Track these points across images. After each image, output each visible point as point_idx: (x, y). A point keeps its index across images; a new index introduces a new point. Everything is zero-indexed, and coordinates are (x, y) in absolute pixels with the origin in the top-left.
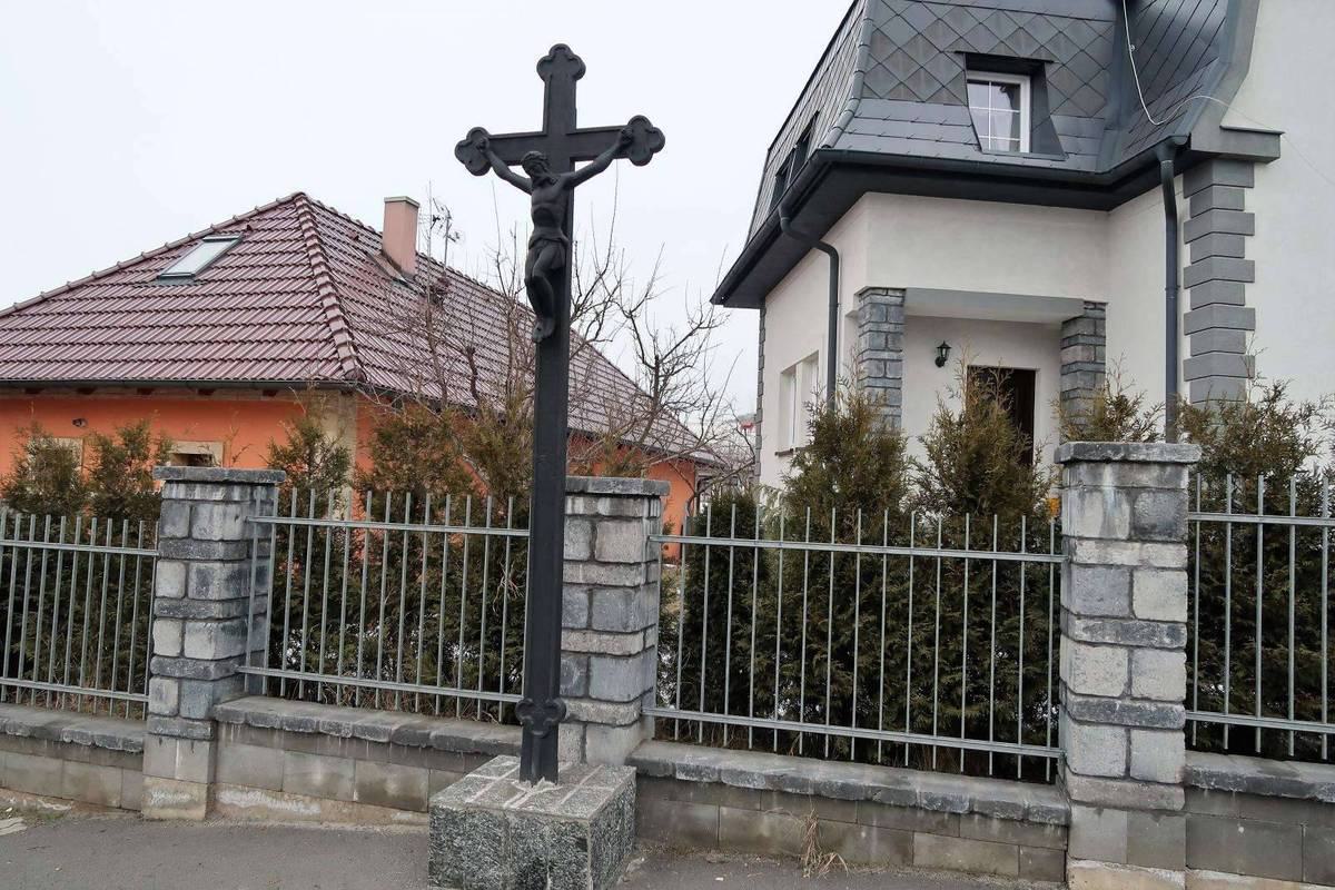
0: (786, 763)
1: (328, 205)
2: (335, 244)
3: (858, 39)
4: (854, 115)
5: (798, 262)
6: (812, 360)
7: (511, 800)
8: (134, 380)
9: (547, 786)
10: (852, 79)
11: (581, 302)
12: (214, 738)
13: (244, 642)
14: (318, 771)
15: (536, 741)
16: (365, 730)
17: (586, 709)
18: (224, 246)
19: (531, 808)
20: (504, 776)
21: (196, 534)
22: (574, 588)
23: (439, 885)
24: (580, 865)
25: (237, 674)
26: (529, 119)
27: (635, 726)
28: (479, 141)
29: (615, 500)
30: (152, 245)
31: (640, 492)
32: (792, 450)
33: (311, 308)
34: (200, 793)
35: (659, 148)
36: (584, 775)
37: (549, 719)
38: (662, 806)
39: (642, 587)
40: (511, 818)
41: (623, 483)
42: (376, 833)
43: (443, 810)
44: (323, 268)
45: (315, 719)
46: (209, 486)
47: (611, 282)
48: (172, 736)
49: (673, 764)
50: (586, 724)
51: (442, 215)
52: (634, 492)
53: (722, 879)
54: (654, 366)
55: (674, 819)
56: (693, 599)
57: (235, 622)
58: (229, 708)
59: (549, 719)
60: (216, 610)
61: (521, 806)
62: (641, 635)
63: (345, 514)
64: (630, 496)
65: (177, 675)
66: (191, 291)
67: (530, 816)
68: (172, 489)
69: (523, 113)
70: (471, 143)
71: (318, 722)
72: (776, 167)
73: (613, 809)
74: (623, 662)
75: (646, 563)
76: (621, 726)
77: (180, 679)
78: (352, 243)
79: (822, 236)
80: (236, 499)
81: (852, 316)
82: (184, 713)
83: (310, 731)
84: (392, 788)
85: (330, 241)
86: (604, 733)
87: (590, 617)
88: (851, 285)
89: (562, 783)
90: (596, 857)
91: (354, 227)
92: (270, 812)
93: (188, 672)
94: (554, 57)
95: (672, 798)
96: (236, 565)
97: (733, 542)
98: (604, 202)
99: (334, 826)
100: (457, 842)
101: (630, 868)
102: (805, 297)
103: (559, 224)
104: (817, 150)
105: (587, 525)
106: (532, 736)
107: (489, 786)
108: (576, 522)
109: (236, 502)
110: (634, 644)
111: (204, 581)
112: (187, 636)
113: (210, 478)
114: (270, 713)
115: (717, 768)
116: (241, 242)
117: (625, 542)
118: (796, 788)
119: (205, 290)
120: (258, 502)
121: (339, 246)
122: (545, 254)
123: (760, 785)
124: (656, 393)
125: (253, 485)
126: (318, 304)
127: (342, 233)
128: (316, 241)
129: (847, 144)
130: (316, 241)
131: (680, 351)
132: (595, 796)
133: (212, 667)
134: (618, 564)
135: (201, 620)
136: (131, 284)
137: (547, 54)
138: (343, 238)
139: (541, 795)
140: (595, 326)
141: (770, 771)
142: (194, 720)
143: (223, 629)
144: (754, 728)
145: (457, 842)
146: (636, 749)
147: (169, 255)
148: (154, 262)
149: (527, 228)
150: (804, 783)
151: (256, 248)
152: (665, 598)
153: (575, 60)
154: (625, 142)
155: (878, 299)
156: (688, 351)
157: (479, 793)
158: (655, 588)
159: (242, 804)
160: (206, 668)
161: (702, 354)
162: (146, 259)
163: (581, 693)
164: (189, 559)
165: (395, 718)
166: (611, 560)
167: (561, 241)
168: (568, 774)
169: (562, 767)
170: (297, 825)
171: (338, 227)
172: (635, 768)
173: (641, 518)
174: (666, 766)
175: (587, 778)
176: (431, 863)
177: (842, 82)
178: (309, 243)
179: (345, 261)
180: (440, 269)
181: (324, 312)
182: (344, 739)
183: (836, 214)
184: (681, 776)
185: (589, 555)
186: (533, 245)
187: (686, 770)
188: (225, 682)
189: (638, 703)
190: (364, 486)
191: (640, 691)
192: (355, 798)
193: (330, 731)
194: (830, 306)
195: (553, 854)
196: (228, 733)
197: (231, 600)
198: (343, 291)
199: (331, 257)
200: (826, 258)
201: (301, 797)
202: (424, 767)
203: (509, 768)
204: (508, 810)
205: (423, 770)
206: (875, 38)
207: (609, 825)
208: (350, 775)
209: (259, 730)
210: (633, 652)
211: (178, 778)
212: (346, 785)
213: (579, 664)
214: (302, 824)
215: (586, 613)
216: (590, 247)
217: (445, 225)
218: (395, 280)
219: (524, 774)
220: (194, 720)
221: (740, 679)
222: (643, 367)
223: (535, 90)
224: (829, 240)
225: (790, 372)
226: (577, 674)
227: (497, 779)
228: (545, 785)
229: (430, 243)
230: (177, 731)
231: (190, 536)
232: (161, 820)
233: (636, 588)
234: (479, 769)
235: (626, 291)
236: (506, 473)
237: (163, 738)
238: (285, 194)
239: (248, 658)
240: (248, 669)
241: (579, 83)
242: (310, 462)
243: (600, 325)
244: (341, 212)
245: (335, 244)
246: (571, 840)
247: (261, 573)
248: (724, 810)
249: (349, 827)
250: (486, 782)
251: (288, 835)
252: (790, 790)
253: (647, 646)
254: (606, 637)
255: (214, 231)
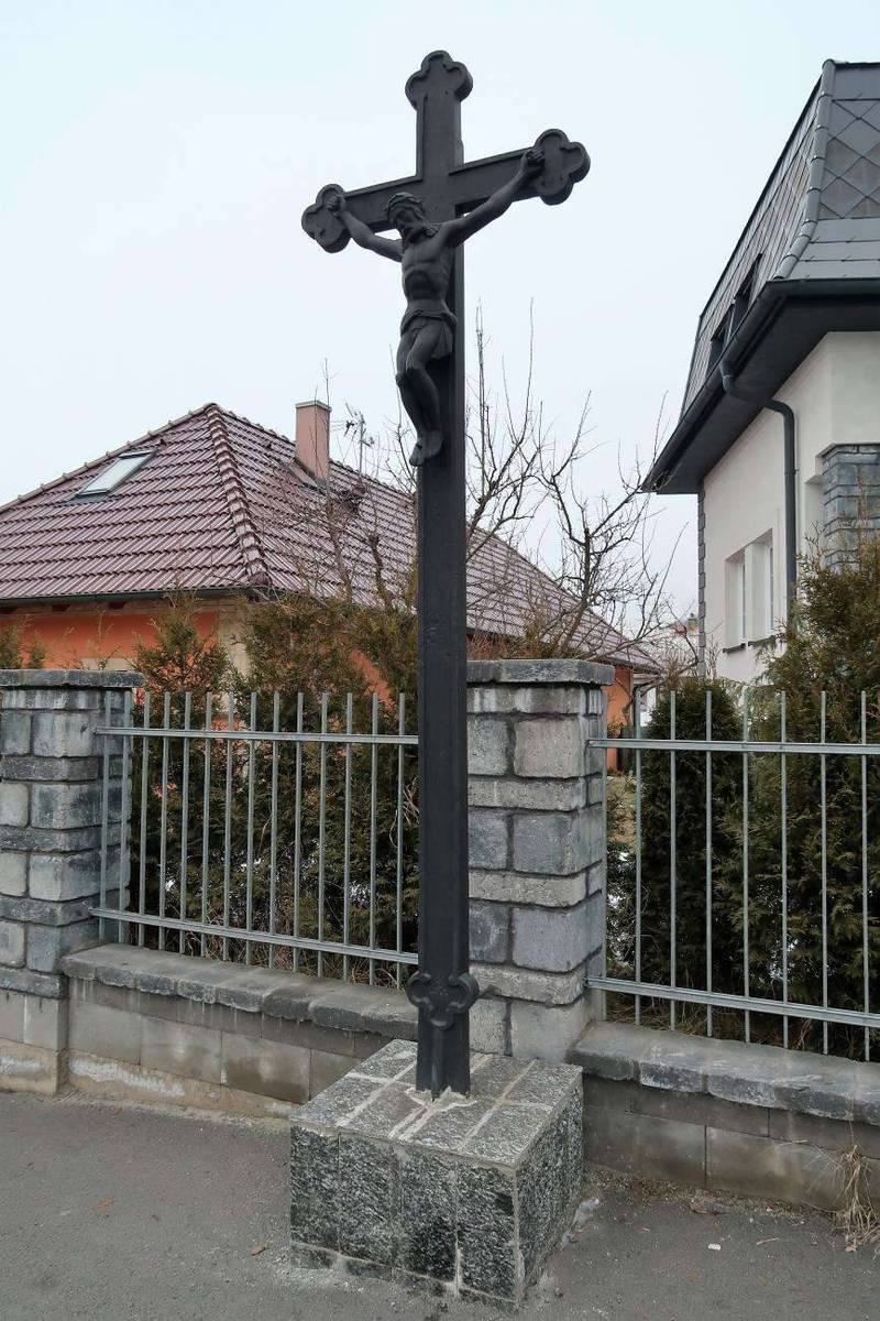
0: (802, 1066)
1: (239, 415)
2: (246, 452)
3: (808, 159)
4: (810, 241)
5: (746, 427)
6: (765, 540)
7: (402, 1125)
8: (48, 597)
9: (456, 1100)
10: (804, 202)
11: (495, 479)
12: (64, 996)
13: (97, 879)
14: (180, 1043)
15: (437, 1035)
16: (231, 995)
17: (511, 982)
18: (139, 460)
19: (428, 1142)
20: (396, 1077)
21: (37, 751)
22: (488, 814)
23: (305, 1241)
24: (503, 1235)
25: (92, 917)
26: (399, 162)
27: (578, 1004)
28: (331, 201)
29: (540, 691)
30: (74, 465)
31: (572, 679)
32: (743, 645)
33: (219, 514)
34: (51, 1063)
35: (581, 172)
36: (507, 1080)
37: (454, 1004)
38: (619, 1119)
39: (580, 811)
40: (400, 1153)
41: (549, 666)
42: (246, 1129)
43: (306, 1134)
44: (231, 474)
45: (173, 978)
46: (49, 692)
47: (528, 449)
48: (19, 991)
49: (636, 1063)
50: (510, 1000)
51: (356, 420)
52: (566, 678)
53: (718, 1247)
54: (583, 541)
55: (638, 1140)
56: (653, 826)
57: (86, 856)
58: (78, 960)
59: (454, 1004)
60: (61, 841)
61: (416, 1137)
62: (582, 877)
63: (232, 731)
64: (559, 685)
65: (23, 918)
66: (106, 506)
67: (427, 1154)
68: (11, 696)
69: (386, 152)
70: (322, 207)
71: (176, 983)
72: (710, 333)
73: (555, 1136)
74: (558, 916)
75: (585, 777)
76: (558, 1006)
77: (26, 923)
78: (264, 450)
79: (775, 392)
80: (82, 707)
81: (815, 483)
82: (31, 964)
83: (168, 993)
84: (266, 1070)
85: (241, 450)
86: (535, 1014)
87: (510, 853)
88: (815, 439)
89: (477, 1093)
90: (528, 1218)
91: (267, 436)
92: (127, 1091)
93: (34, 915)
94: (428, 71)
95: (636, 1109)
96: (85, 788)
97: (709, 745)
98: (503, 258)
99: (201, 1114)
100: (327, 1183)
101: (580, 1217)
102: (754, 472)
103: (442, 294)
104: (767, 283)
105: (501, 726)
106: (431, 1027)
107: (375, 1094)
108: (486, 723)
109: (81, 711)
110: (574, 890)
111: (48, 809)
112: (32, 872)
113: (49, 683)
114: (124, 968)
115: (701, 1072)
116: (154, 456)
117: (556, 748)
118: (826, 1109)
119: (119, 505)
120: (108, 710)
121: (251, 454)
122: (423, 337)
123: (769, 1101)
124: (587, 573)
125: (102, 690)
126: (225, 510)
127: (254, 442)
128: (225, 448)
129: (802, 272)
130: (225, 448)
131: (614, 520)
132: (523, 1121)
133: (59, 909)
134: (546, 780)
135: (45, 853)
136: (52, 504)
137: (419, 68)
138: (256, 447)
139: (445, 1116)
140: (513, 501)
141: (783, 1081)
142: (41, 973)
143: (72, 864)
144: (751, 1012)
145: (327, 1183)
146: (581, 1036)
147: (87, 474)
148: (74, 482)
149: (400, 305)
150: (840, 1104)
151: (168, 461)
152: (613, 822)
153: (458, 69)
154: (532, 169)
155: (847, 457)
156: (624, 519)
157: (359, 1109)
158: (600, 812)
159: (97, 1078)
160: (52, 911)
161: (641, 523)
162: (67, 480)
163: (501, 958)
164: (32, 780)
165: (271, 979)
166: (537, 775)
167: (445, 318)
168: (485, 1075)
169: (477, 1063)
170: (157, 1109)
171: (249, 436)
172: (580, 1069)
173: (576, 715)
174: (625, 1065)
175: (512, 1084)
176: (293, 1207)
177: (791, 208)
178: (218, 451)
179: (256, 473)
180: (356, 477)
181: (231, 518)
182: (207, 1005)
183: (790, 365)
184: (648, 1081)
185: (505, 767)
186: (407, 327)
187: (654, 1072)
188: (76, 928)
189: (582, 972)
190: (243, 690)
191: (584, 955)
192: (224, 1080)
193: (189, 994)
194: (786, 473)
195: (462, 1214)
196: (80, 990)
197: (81, 828)
198: (250, 496)
199: (241, 464)
200: (776, 421)
201: (160, 1074)
202: (302, 1045)
203: (404, 1062)
204: (395, 1143)
205: (303, 1050)
206: (833, 148)
207: (545, 1164)
208: (217, 1050)
209: (115, 990)
210: (572, 903)
211: (26, 1041)
212: (212, 1062)
213: (498, 919)
214: (160, 1109)
215: (504, 848)
216: (503, 410)
217: (359, 431)
218: (306, 485)
219: (423, 1079)
220: (41, 973)
221: (727, 934)
222: (570, 543)
223: (405, 119)
224: (784, 397)
225: (737, 559)
226: (495, 932)
227: (386, 1081)
228: (452, 1100)
229: (342, 448)
230: (24, 985)
231: (31, 753)
232: (11, 1091)
233: (572, 812)
234: (364, 1064)
235: (546, 456)
236: (403, 667)
237: (11, 993)
238: (197, 406)
239: (103, 899)
240: (103, 912)
241: (464, 103)
242: (182, 664)
243: (519, 499)
244: (253, 422)
245: (246, 452)
246: (489, 1196)
247: (115, 797)
248: (713, 1133)
249: (216, 1117)
250: (371, 1087)
251: (145, 1124)
252: (815, 1112)
253: (591, 892)
254: (532, 881)
255: (131, 447)
